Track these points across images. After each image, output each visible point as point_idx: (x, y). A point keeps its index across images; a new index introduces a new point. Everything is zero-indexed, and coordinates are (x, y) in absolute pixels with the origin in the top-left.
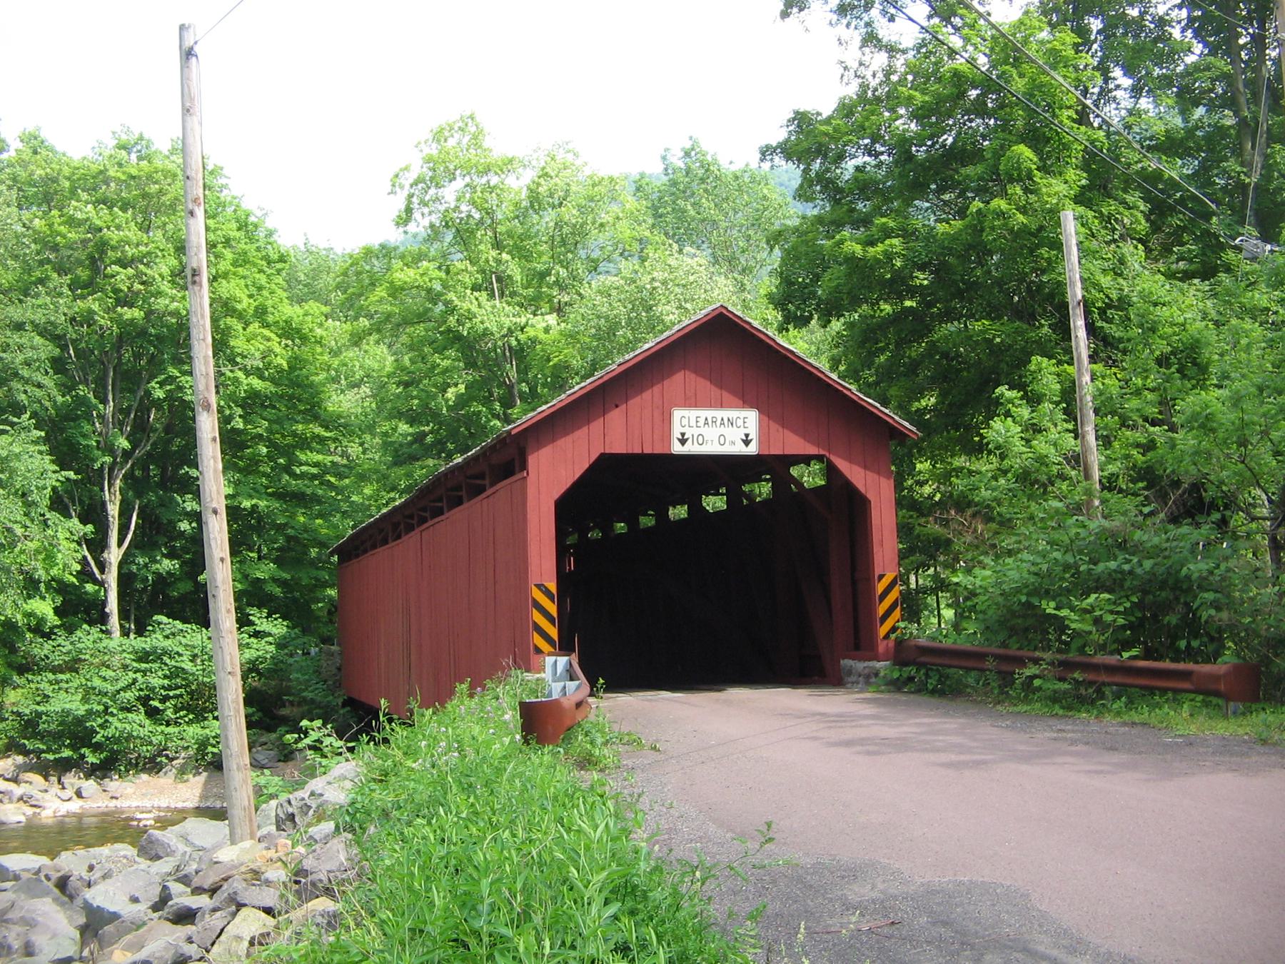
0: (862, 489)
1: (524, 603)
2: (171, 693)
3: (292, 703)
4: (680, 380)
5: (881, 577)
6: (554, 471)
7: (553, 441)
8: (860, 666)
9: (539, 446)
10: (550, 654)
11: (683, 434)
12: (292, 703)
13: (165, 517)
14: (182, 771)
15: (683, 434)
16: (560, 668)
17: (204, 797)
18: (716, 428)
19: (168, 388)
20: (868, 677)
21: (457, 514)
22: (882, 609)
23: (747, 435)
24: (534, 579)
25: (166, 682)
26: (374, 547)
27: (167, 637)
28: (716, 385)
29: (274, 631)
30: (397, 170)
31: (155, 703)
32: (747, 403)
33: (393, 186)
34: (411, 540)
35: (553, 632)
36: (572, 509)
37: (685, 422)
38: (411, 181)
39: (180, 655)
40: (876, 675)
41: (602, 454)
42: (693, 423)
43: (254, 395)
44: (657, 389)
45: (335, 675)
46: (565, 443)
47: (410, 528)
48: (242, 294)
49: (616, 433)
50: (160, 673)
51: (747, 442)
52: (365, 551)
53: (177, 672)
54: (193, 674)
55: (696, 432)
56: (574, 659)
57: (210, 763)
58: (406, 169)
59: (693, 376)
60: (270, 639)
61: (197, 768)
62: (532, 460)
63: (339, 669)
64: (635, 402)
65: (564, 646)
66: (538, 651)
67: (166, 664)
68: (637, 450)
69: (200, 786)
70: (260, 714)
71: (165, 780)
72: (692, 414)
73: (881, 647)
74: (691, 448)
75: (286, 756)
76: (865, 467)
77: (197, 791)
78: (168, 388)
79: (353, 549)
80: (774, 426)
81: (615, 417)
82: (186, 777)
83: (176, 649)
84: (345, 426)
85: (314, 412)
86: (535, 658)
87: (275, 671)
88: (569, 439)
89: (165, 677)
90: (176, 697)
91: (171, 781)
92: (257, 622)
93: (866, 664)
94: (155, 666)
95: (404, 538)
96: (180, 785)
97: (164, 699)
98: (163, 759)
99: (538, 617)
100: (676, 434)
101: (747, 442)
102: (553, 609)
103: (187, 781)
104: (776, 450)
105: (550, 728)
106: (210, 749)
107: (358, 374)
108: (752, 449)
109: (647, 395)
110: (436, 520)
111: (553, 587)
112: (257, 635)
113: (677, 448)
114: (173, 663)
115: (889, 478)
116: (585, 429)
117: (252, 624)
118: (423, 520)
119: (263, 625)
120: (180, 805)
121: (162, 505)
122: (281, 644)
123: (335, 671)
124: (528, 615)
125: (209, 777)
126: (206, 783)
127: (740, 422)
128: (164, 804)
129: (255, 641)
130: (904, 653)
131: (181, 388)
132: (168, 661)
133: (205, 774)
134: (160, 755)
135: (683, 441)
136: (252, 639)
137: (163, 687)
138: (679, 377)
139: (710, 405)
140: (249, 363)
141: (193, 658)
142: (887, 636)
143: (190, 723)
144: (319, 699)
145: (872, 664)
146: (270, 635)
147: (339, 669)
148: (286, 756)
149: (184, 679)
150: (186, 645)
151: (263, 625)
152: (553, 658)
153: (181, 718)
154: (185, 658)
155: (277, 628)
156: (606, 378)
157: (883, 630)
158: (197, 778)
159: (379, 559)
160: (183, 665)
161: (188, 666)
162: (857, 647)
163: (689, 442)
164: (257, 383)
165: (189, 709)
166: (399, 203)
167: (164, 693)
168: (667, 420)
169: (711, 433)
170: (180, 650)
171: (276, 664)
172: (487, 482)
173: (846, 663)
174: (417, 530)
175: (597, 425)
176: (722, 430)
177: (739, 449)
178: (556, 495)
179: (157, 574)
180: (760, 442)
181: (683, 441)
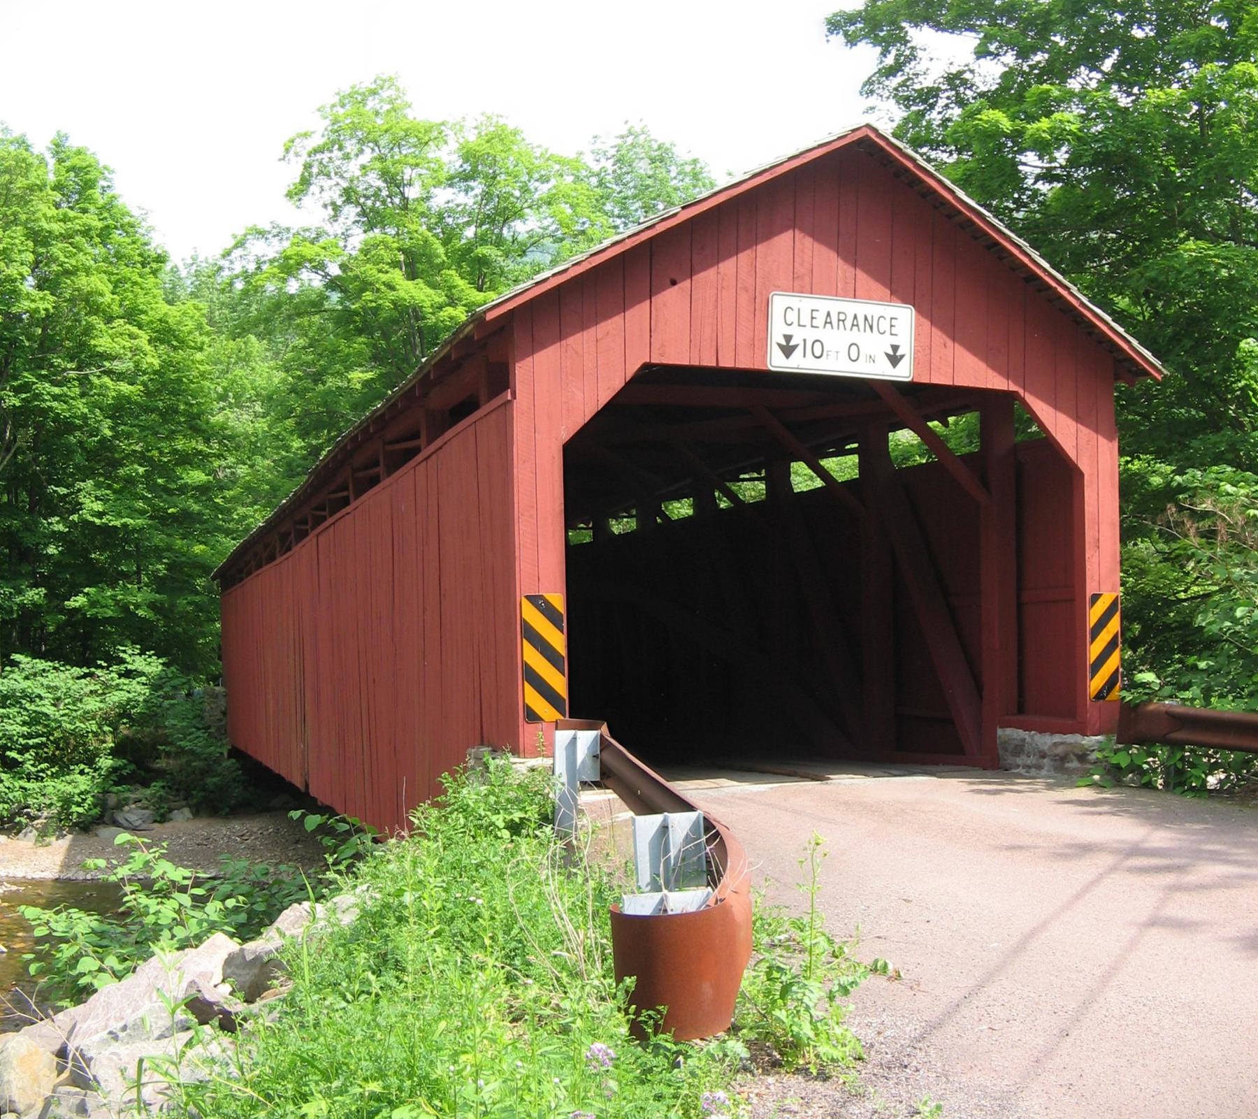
0: (1072, 454)
1: (504, 630)
2: (31, 742)
3: (168, 754)
4: (785, 248)
5: (1096, 598)
6: (560, 391)
7: (561, 337)
8: (1045, 741)
9: (535, 346)
10: (557, 726)
11: (788, 338)
12: (168, 754)
13: (29, 540)
14: (43, 833)
15: (788, 338)
16: (582, 752)
17: (66, 866)
18: (845, 328)
19: (24, 396)
20: (1063, 758)
21: (370, 498)
22: (1095, 650)
23: (895, 348)
24: (525, 584)
25: (25, 729)
26: (259, 566)
27: (27, 678)
28: (846, 259)
29: (147, 669)
30: (292, 135)
31: (13, 754)
32: (899, 291)
33: (287, 151)
34: (304, 551)
35: (559, 682)
36: (602, 462)
37: (792, 317)
38: (310, 149)
39: (41, 698)
40: (1082, 758)
41: (647, 367)
42: (805, 320)
43: (122, 400)
44: (744, 257)
45: (220, 720)
46: (581, 342)
47: (302, 535)
48: (106, 288)
49: (674, 329)
50: (18, 720)
51: (894, 360)
52: (250, 573)
53: (36, 719)
54: (55, 720)
55: (811, 334)
56: (604, 729)
57: (76, 824)
58: (306, 135)
59: (808, 241)
60: (144, 678)
61: (61, 829)
62: (523, 371)
63: (224, 713)
64: (707, 277)
65: (581, 708)
66: (532, 717)
67: (25, 709)
68: (709, 362)
69: (63, 851)
70: (133, 767)
71: (25, 842)
72: (805, 304)
73: (1092, 713)
74: (800, 363)
75: (162, 816)
76: (1078, 419)
77: (59, 858)
78: (24, 396)
79: (235, 572)
80: (939, 336)
81: (672, 301)
82: (47, 839)
83: (37, 691)
84: (231, 438)
85: (196, 425)
86: (527, 732)
87: (151, 717)
88: (588, 336)
89: (24, 723)
90: (36, 746)
91: (31, 844)
92: (129, 659)
93: (1058, 738)
94: (13, 711)
95: (295, 549)
96: (41, 850)
97: (24, 750)
98: (24, 820)
99: (532, 656)
100: (777, 336)
101: (894, 360)
102: (558, 640)
103: (49, 844)
104: (940, 378)
105: (707, 988)
106: (74, 808)
107: (246, 386)
108: (903, 373)
109: (728, 266)
110: (339, 515)
111: (558, 601)
112: (128, 674)
113: (777, 362)
114: (33, 707)
115: (1111, 439)
116: (618, 319)
117: (123, 661)
118: (319, 521)
119: (138, 663)
120: (38, 875)
121: (28, 529)
122: (156, 686)
123: (220, 716)
124: (512, 652)
125: (73, 840)
126: (70, 848)
127: (884, 325)
128: (20, 874)
129: (127, 681)
130: (1134, 725)
131: (37, 396)
132: (27, 705)
133: (70, 837)
134: (19, 814)
135: (788, 350)
136: (123, 680)
137: (24, 736)
138: (783, 241)
139: (834, 291)
140: (118, 366)
141: (56, 702)
142: (1100, 696)
143: (54, 776)
144: (199, 750)
145: (1070, 738)
146: (142, 674)
147: (224, 713)
148: (162, 816)
149: (46, 726)
150: (48, 687)
151: (138, 663)
152: (570, 733)
153: (42, 771)
154: (46, 702)
155: (151, 665)
156: (660, 228)
157: (1096, 683)
158: (60, 841)
159: (264, 581)
160: (44, 710)
161: (50, 710)
162: (1021, 709)
163: (799, 351)
164: (125, 388)
165: (52, 760)
166: (293, 172)
167: (23, 742)
168: (762, 312)
169: (836, 340)
170: (43, 692)
171: (148, 708)
172: (422, 441)
173: (1009, 734)
174: (313, 534)
175: (638, 314)
176: (855, 336)
177: (880, 370)
178: (565, 434)
179: (22, 606)
180: (917, 362)
181: (788, 350)
